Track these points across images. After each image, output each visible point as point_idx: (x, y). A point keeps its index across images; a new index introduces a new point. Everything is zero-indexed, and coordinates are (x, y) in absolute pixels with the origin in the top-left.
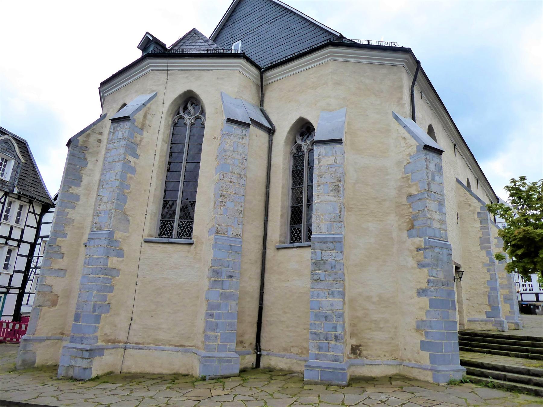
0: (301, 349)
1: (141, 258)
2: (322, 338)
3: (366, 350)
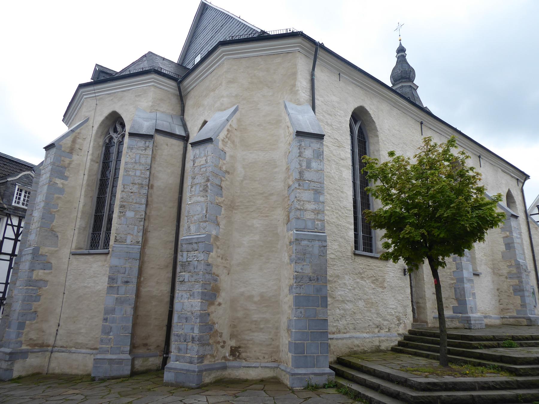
1: (69, 269)
2: (182, 340)
3: (246, 352)
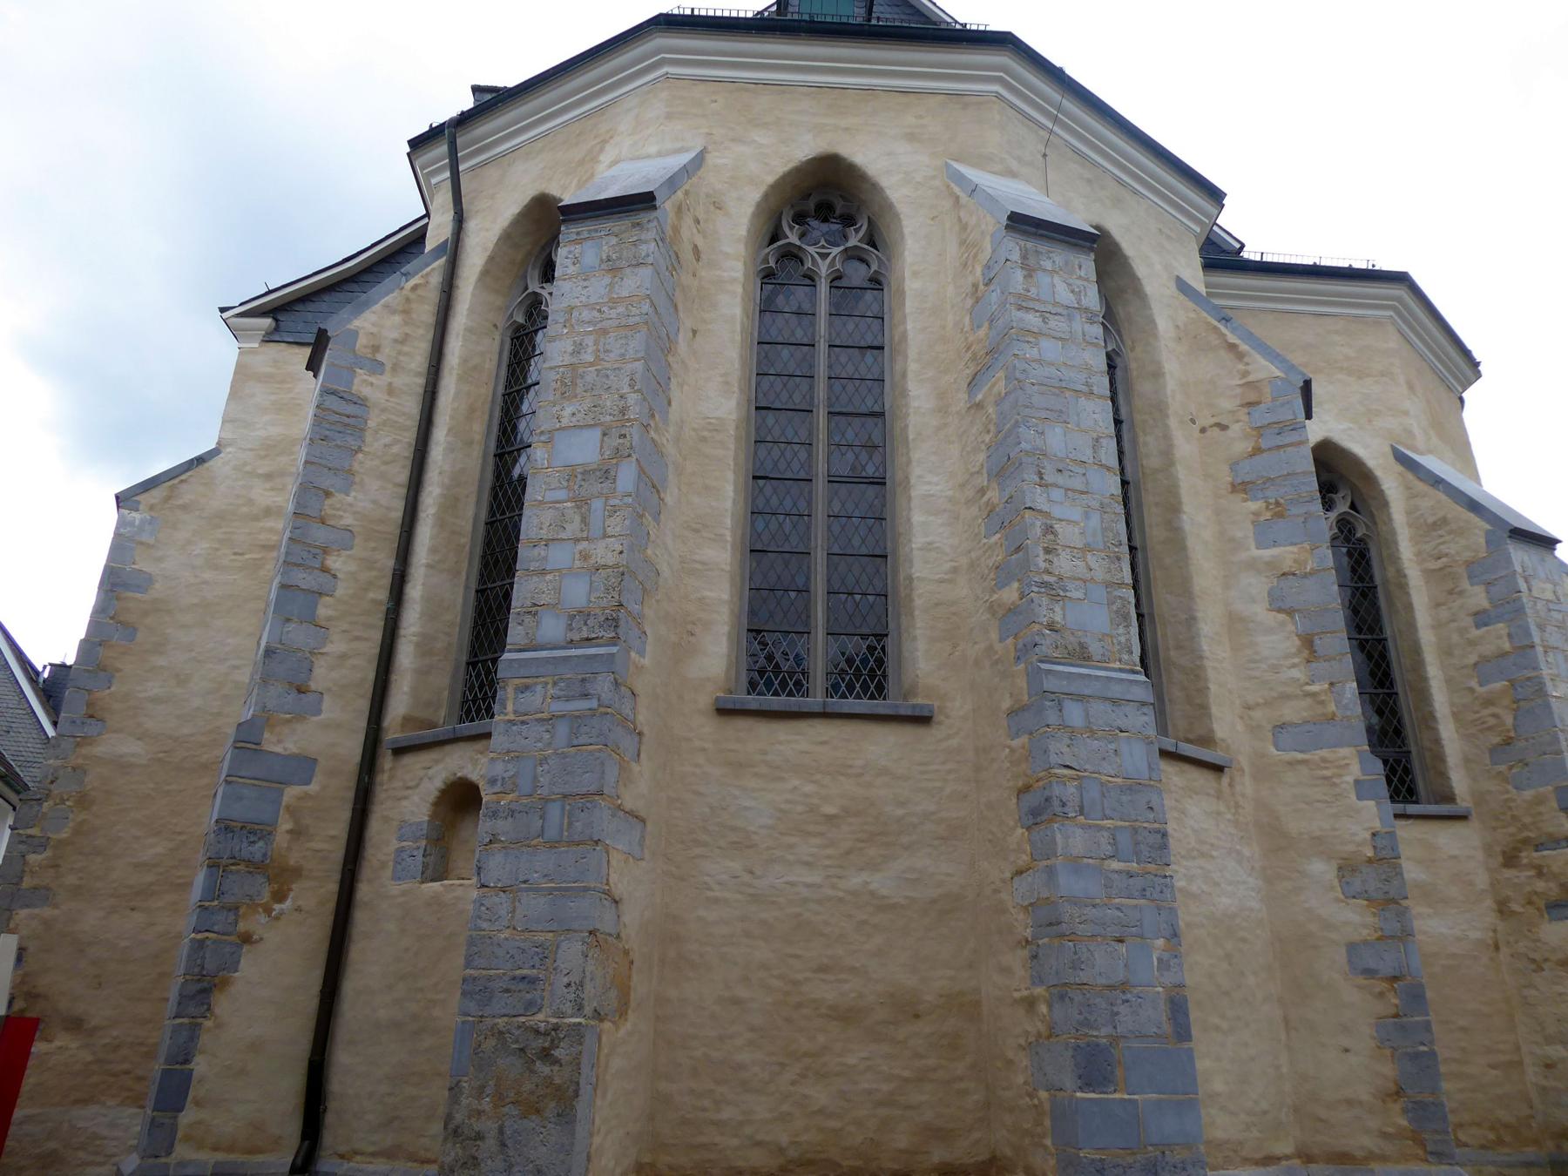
0: (1492, 1128)
